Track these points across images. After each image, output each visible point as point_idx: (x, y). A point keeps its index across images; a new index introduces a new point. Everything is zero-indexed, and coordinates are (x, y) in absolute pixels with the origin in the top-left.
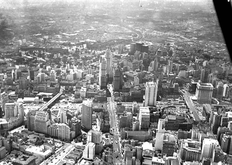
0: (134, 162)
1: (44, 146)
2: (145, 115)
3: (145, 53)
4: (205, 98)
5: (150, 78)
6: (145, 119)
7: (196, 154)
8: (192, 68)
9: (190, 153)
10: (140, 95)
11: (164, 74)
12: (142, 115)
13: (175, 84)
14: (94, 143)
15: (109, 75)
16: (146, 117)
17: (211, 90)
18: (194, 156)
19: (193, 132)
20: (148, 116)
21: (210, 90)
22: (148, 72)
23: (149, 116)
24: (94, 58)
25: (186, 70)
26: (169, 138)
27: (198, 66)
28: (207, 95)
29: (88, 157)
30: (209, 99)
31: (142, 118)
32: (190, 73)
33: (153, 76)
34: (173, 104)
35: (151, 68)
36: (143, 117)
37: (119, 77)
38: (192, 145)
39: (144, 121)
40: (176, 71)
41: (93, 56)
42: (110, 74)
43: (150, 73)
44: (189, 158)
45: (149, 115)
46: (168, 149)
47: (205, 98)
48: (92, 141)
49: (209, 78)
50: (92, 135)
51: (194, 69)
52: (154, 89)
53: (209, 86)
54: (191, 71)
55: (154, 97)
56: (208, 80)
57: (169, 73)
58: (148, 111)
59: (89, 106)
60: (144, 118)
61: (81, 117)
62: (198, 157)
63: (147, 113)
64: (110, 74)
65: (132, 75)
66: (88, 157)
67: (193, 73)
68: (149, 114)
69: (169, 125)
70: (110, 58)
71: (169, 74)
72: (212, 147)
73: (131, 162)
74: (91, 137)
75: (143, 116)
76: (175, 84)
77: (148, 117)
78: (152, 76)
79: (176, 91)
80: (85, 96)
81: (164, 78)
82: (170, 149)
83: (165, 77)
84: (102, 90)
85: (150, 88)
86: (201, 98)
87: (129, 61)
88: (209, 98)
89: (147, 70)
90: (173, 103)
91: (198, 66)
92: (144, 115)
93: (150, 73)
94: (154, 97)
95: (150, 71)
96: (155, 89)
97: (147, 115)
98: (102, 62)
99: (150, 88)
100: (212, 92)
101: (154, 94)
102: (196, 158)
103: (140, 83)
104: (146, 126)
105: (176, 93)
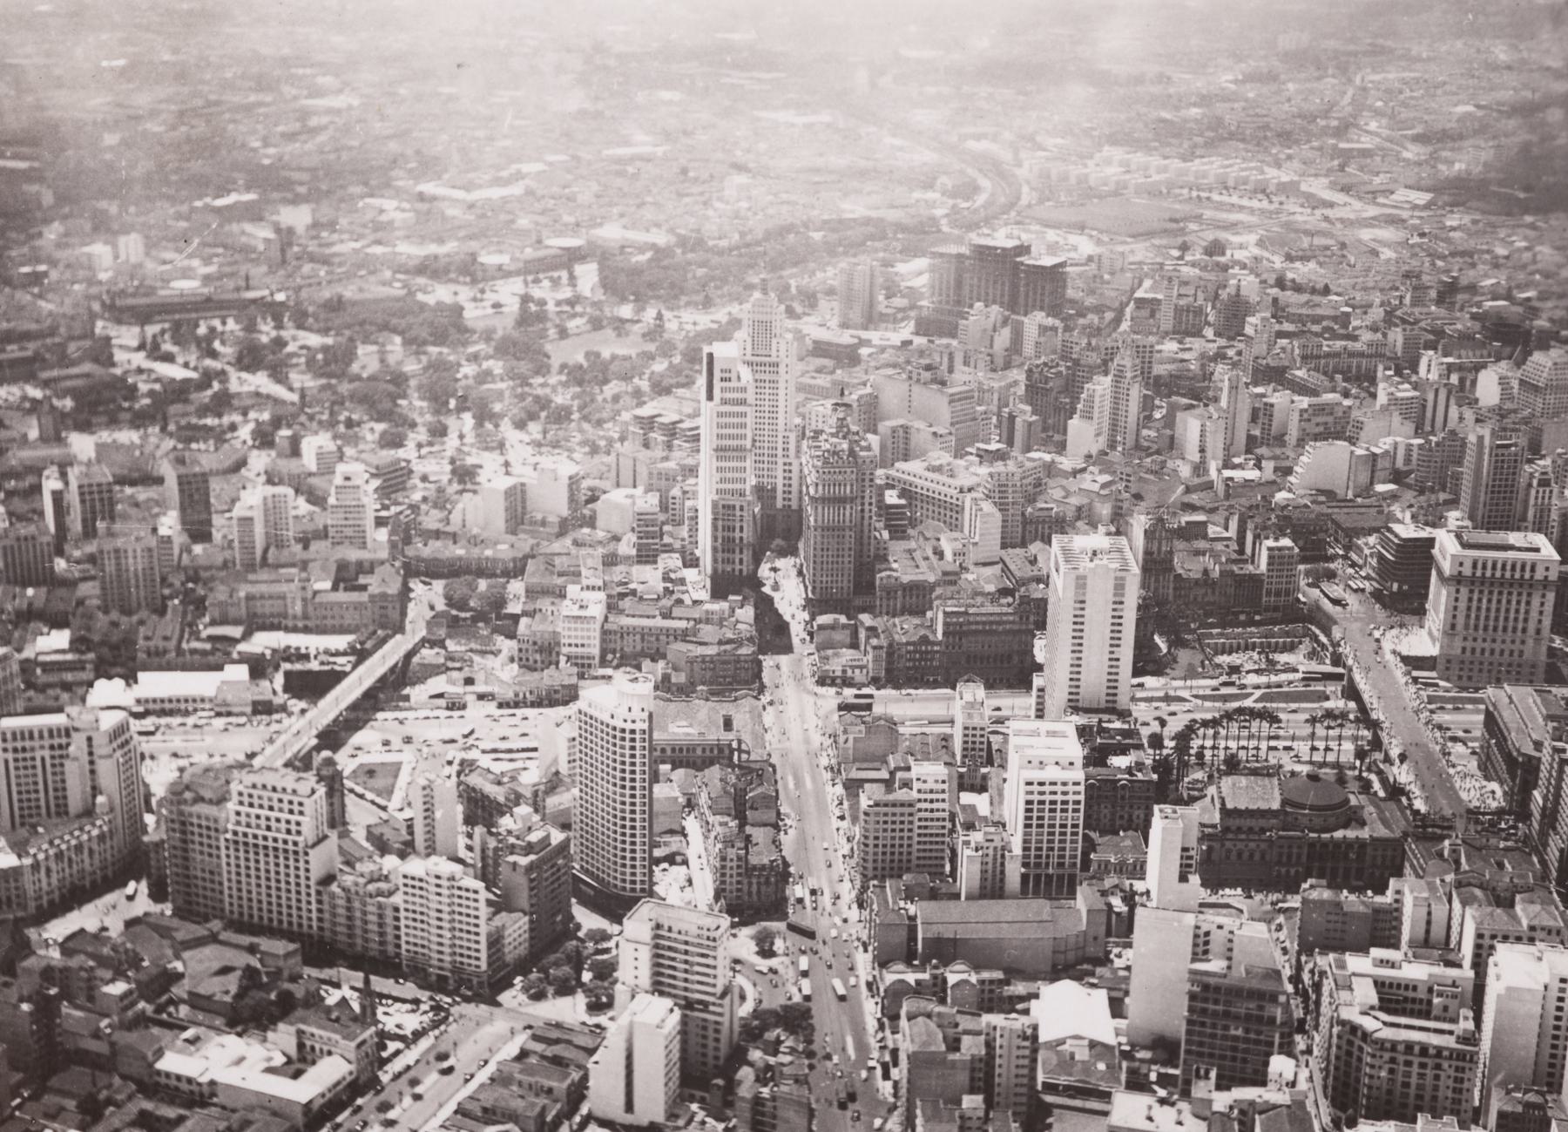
5: (1079, 509)
9: (1393, 1060)
11: (1185, 471)
13: (1270, 543)
17: (1545, 584)
20: (1070, 788)
21: (1532, 584)
22: (1066, 463)
23: (1082, 788)
29: (629, 1107)
31: (1029, 802)
32: (1380, 464)
34: (1258, 693)
37: (852, 500)
38: (1410, 994)
40: (1278, 451)
41: (652, 347)
43: (1083, 470)
44: (1389, 1092)
46: (1226, 1028)
48: (658, 988)
55: (1115, 642)
58: (1075, 750)
62: (1450, 1083)
63: (1065, 762)
65: (942, 486)
66: (629, 1107)
67: (1408, 460)
71: (1227, 473)
74: (645, 954)
75: (1036, 788)
76: (1270, 543)
78: (1096, 487)
81: (1186, 499)
82: (1240, 1032)
83: (1194, 498)
88: (1530, 642)
89: (1061, 447)
93: (1083, 470)
99: (1081, 583)
100: (1551, 597)
102: (1440, 1094)
103: (1004, 546)
105: (1276, 609)
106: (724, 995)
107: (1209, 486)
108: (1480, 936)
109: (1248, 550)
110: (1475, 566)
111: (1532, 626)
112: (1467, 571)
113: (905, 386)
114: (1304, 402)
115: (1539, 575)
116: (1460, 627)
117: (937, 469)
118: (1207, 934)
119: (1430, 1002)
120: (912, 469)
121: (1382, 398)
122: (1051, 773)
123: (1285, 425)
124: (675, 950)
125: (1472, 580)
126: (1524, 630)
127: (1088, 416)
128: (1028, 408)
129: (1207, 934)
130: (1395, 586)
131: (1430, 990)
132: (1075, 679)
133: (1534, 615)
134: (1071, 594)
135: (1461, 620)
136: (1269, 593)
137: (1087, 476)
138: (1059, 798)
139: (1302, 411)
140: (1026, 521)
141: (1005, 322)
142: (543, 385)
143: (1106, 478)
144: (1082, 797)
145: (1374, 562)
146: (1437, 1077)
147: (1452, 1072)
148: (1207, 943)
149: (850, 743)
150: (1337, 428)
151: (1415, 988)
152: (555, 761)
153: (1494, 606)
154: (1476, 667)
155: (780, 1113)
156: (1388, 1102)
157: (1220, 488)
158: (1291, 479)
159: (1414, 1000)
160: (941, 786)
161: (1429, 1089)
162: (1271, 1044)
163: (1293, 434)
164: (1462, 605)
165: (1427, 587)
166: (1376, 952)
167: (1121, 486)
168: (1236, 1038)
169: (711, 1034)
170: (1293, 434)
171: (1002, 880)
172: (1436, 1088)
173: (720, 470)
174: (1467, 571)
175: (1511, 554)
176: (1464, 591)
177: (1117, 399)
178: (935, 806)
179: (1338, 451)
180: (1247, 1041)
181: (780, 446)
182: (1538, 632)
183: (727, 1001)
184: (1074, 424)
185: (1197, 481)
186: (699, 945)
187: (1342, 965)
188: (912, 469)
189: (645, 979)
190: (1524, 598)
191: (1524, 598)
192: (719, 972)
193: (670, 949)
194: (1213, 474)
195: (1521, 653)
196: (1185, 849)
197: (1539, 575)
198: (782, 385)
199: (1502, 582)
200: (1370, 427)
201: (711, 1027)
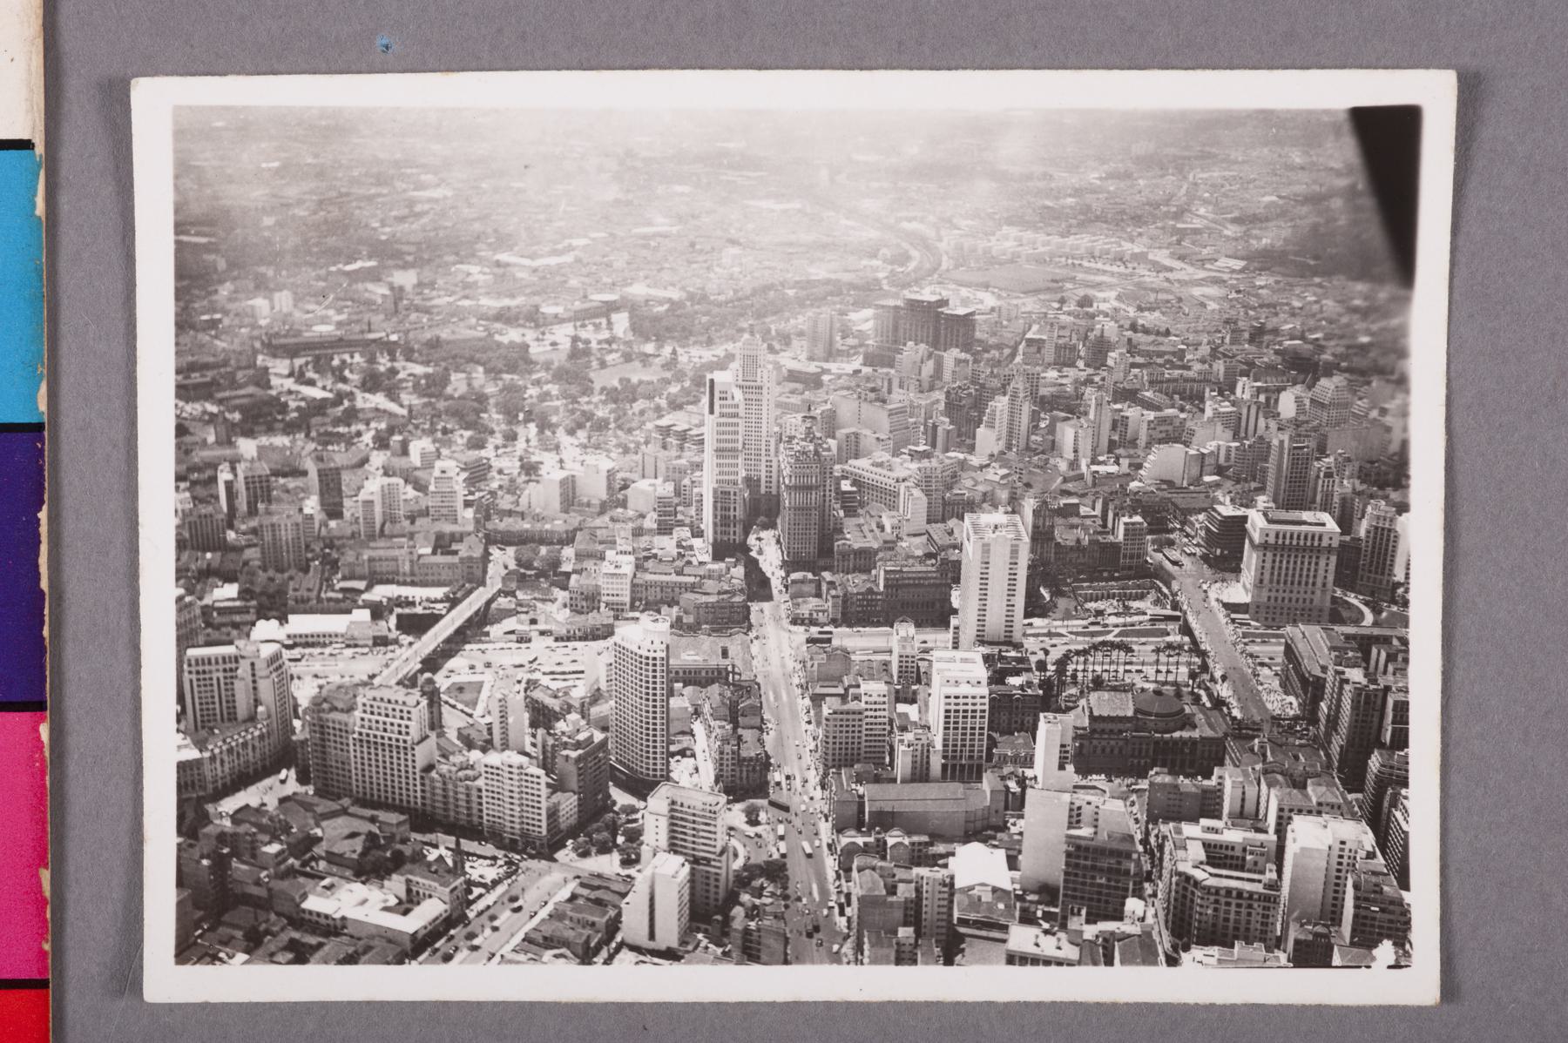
5: (985, 494)
7: (1250, 906)
8: (1219, 428)
9: (1217, 902)
11: (1063, 466)
13: (1126, 519)
14: (681, 859)
17: (1329, 549)
18: (1238, 913)
19: (1229, 780)
20: (978, 700)
21: (1319, 550)
22: (975, 460)
23: (986, 701)
24: (674, 389)
33: (1003, 477)
34: (1117, 630)
38: (1230, 853)
40: (1132, 452)
41: (668, 375)
42: (763, 474)
44: (1214, 925)
46: (1093, 878)
48: (673, 848)
52: (1008, 549)
54: (1210, 447)
55: (1011, 592)
58: (981, 672)
62: (1259, 918)
63: (974, 682)
66: (652, 936)
67: (1228, 458)
71: (1094, 468)
74: (664, 824)
75: (953, 700)
78: (997, 478)
81: (1064, 487)
82: (1103, 881)
83: (1070, 486)
85: (986, 549)
88: (1318, 593)
99: (986, 549)
100: (1334, 559)
102: (1252, 927)
105: (1130, 568)
106: (722, 853)
107: (1081, 477)
108: (1281, 810)
109: (1110, 525)
112: (1272, 540)
114: (1151, 415)
115: (1325, 543)
116: (1266, 581)
119: (1244, 859)
120: (861, 465)
121: (1209, 413)
122: (964, 689)
123: (1137, 432)
125: (1275, 547)
127: (991, 426)
131: (1244, 850)
132: (981, 620)
133: (1321, 572)
136: (1125, 556)
138: (970, 707)
140: (945, 503)
144: (986, 707)
145: (1203, 533)
146: (1249, 914)
150: (1174, 434)
152: (597, 680)
155: (763, 941)
156: (1214, 932)
157: (1089, 479)
162: (1127, 890)
163: (1142, 441)
164: (1268, 565)
166: (1204, 822)
167: (1015, 477)
168: (1100, 885)
170: (1142, 441)
172: (1248, 922)
174: (1272, 540)
175: (1304, 528)
176: (1269, 555)
177: (1013, 413)
180: (1108, 887)
182: (1324, 585)
183: (724, 858)
184: (981, 431)
188: (861, 465)
189: (663, 841)
194: (1084, 469)
196: (1063, 746)
197: (1325, 543)
198: (765, 403)
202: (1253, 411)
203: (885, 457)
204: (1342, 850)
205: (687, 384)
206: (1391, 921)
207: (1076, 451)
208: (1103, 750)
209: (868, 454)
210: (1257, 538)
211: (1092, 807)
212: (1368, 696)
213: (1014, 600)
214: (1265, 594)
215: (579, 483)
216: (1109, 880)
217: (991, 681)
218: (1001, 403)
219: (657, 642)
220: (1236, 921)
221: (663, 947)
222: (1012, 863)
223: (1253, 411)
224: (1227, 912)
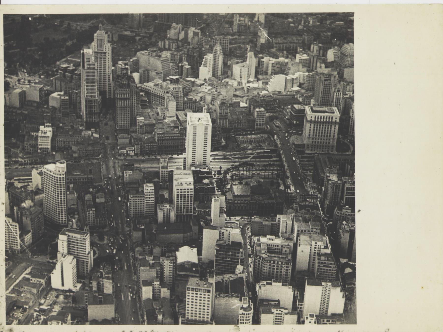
0: (157, 288)
1: (155, 270)
2: (185, 189)
3: (193, 29)
4: (325, 141)
5: (201, 98)
6: (185, 197)
7: (282, 267)
8: (301, 66)
9: (270, 265)
10: (178, 139)
11: (235, 84)
12: (178, 189)
13: (257, 110)
14: (72, 257)
15: (105, 91)
16: (183, 193)
17: (336, 123)
18: (277, 269)
19: (284, 220)
20: (190, 191)
21: (332, 123)
22: (198, 82)
23: (193, 190)
24: (69, 43)
25: (287, 74)
26: (230, 235)
27: (315, 61)
28: (323, 134)
29: (63, 285)
30: (331, 142)
31: (177, 195)
32: (295, 81)
33: (209, 90)
34: (252, 156)
35: (206, 69)
36: (180, 193)
37: (129, 99)
38: (276, 247)
39: (181, 201)
40: (264, 77)
41: (66, 36)
42: (107, 89)
43: (203, 84)
44: (269, 273)
45: (191, 189)
46: (226, 258)
47: (322, 141)
48: (69, 253)
49: (332, 94)
50: (68, 239)
51: (305, 69)
52: (204, 128)
53: (331, 115)
54: (297, 75)
55: (205, 146)
56: (331, 99)
57: (248, 82)
58: (191, 179)
59: (59, 176)
60: (181, 195)
61: (42, 199)
62: (285, 271)
63: (188, 183)
64: (107, 89)
65: (159, 92)
66: (63, 285)
67: (304, 79)
68: (192, 187)
69: (236, 207)
70: (105, 53)
71: (248, 85)
72: (315, 248)
73: (151, 290)
74: (65, 244)
75: (180, 191)
76: (257, 110)
77: (190, 193)
78: (206, 91)
79: (260, 125)
80: (49, 147)
81: (235, 93)
82: (230, 259)
83: (237, 93)
84: (90, 132)
85: (195, 128)
86: (314, 140)
87: (154, 57)
88: (331, 140)
89: (197, 76)
90: (252, 154)
91: (315, 61)
92: (181, 190)
93: (203, 84)
94: (205, 146)
95: (203, 79)
96: (206, 129)
97: (188, 189)
98: (86, 65)
99: (195, 128)
100: (337, 127)
101: (206, 139)
102: (282, 274)
103: (177, 110)
104: (187, 212)
105: (259, 129)
106: (88, 254)
107: (243, 88)
108: (298, 231)
109: (321, 51)
110: (315, 118)
111: (332, 137)
112: (313, 119)
113: (148, 57)
114: (273, 60)
115: (334, 120)
116: (311, 136)
117: (157, 85)
118: (223, 233)
119: (282, 250)
120: (150, 85)
121: (297, 60)
122: (185, 186)
123: (267, 68)
124: (74, 242)
125: (315, 122)
126: (330, 136)
127: (205, 66)
128: (187, 63)
129: (223, 233)
130: (295, 122)
131: (282, 246)
132: (194, 157)
133: (332, 132)
134: (192, 132)
135: (312, 133)
136: (257, 125)
137: (204, 86)
138: (186, 193)
139: (273, 64)
140: (184, 103)
141: (183, 30)
142: (30, 50)
143: (210, 87)
144: (193, 193)
145: (289, 114)
146: (281, 269)
147: (285, 268)
148: (223, 235)
149: (128, 175)
150: (281, 69)
151: (278, 246)
152: (37, 185)
153: (321, 129)
154: (316, 147)
155: (105, 285)
156: (269, 276)
157: (246, 89)
158: (268, 86)
159: (278, 249)
160: (152, 191)
161: (279, 272)
162: (238, 262)
163: (270, 72)
164: (312, 129)
165: (303, 122)
166: (268, 237)
167: (214, 90)
168: (229, 261)
169: (85, 264)
170: (270, 72)
171: (169, 218)
172: (281, 272)
173: (87, 86)
174: (313, 119)
175: (326, 114)
176: (312, 125)
177: (215, 59)
178: (151, 197)
179: (281, 77)
180: (231, 261)
181: (107, 78)
182: (334, 136)
183: (89, 255)
184: (202, 68)
185: (238, 87)
186: (80, 241)
187: (259, 240)
188: (150, 85)
189: (66, 251)
190: (330, 127)
191: (330, 127)
192: (87, 248)
193: (73, 242)
194: (244, 85)
195: (329, 143)
196: (221, 208)
197: (334, 120)
198: (107, 59)
199: (323, 122)
200: (293, 69)
201: (85, 262)
202: (315, 59)
203: (160, 82)
204: (316, 245)
205: (75, 41)
206: (330, 270)
207: (241, 77)
208: (239, 207)
209: (152, 80)
210: (309, 119)
211: (228, 232)
212: (337, 186)
213: (206, 148)
214: (311, 140)
215: (27, 93)
216: (231, 259)
217: (195, 182)
218: (209, 57)
219: (61, 171)
220: (277, 272)
221: (67, 289)
222: (199, 253)
223: (315, 59)
224: (274, 269)
